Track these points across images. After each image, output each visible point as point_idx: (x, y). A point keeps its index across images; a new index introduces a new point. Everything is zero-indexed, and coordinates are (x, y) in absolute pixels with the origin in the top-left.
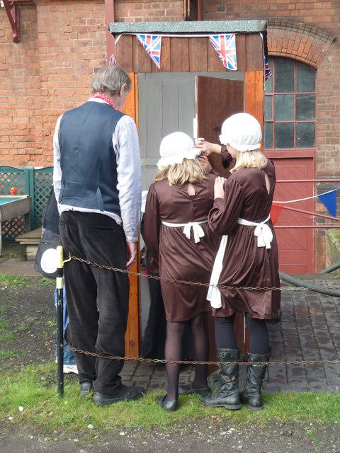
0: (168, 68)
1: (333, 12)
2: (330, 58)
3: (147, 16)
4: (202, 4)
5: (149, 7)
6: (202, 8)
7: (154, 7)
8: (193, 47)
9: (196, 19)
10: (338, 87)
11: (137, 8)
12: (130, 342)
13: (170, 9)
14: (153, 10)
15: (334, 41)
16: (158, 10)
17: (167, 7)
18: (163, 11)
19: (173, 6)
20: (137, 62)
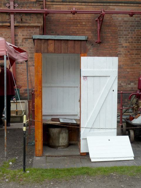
0: (54, 52)
1: (92, 35)
2: (91, 51)
3: (26, 34)
4: (46, 30)
5: (27, 31)
6: (46, 32)
7: (29, 30)
8: (62, 45)
9: (44, 35)
10: (140, 49)
11: (23, 31)
12: (39, 150)
13: (35, 31)
14: (29, 32)
15: (92, 45)
16: (31, 32)
17: (34, 31)
18: (32, 33)
19: (36, 31)
20: (42, 49)
